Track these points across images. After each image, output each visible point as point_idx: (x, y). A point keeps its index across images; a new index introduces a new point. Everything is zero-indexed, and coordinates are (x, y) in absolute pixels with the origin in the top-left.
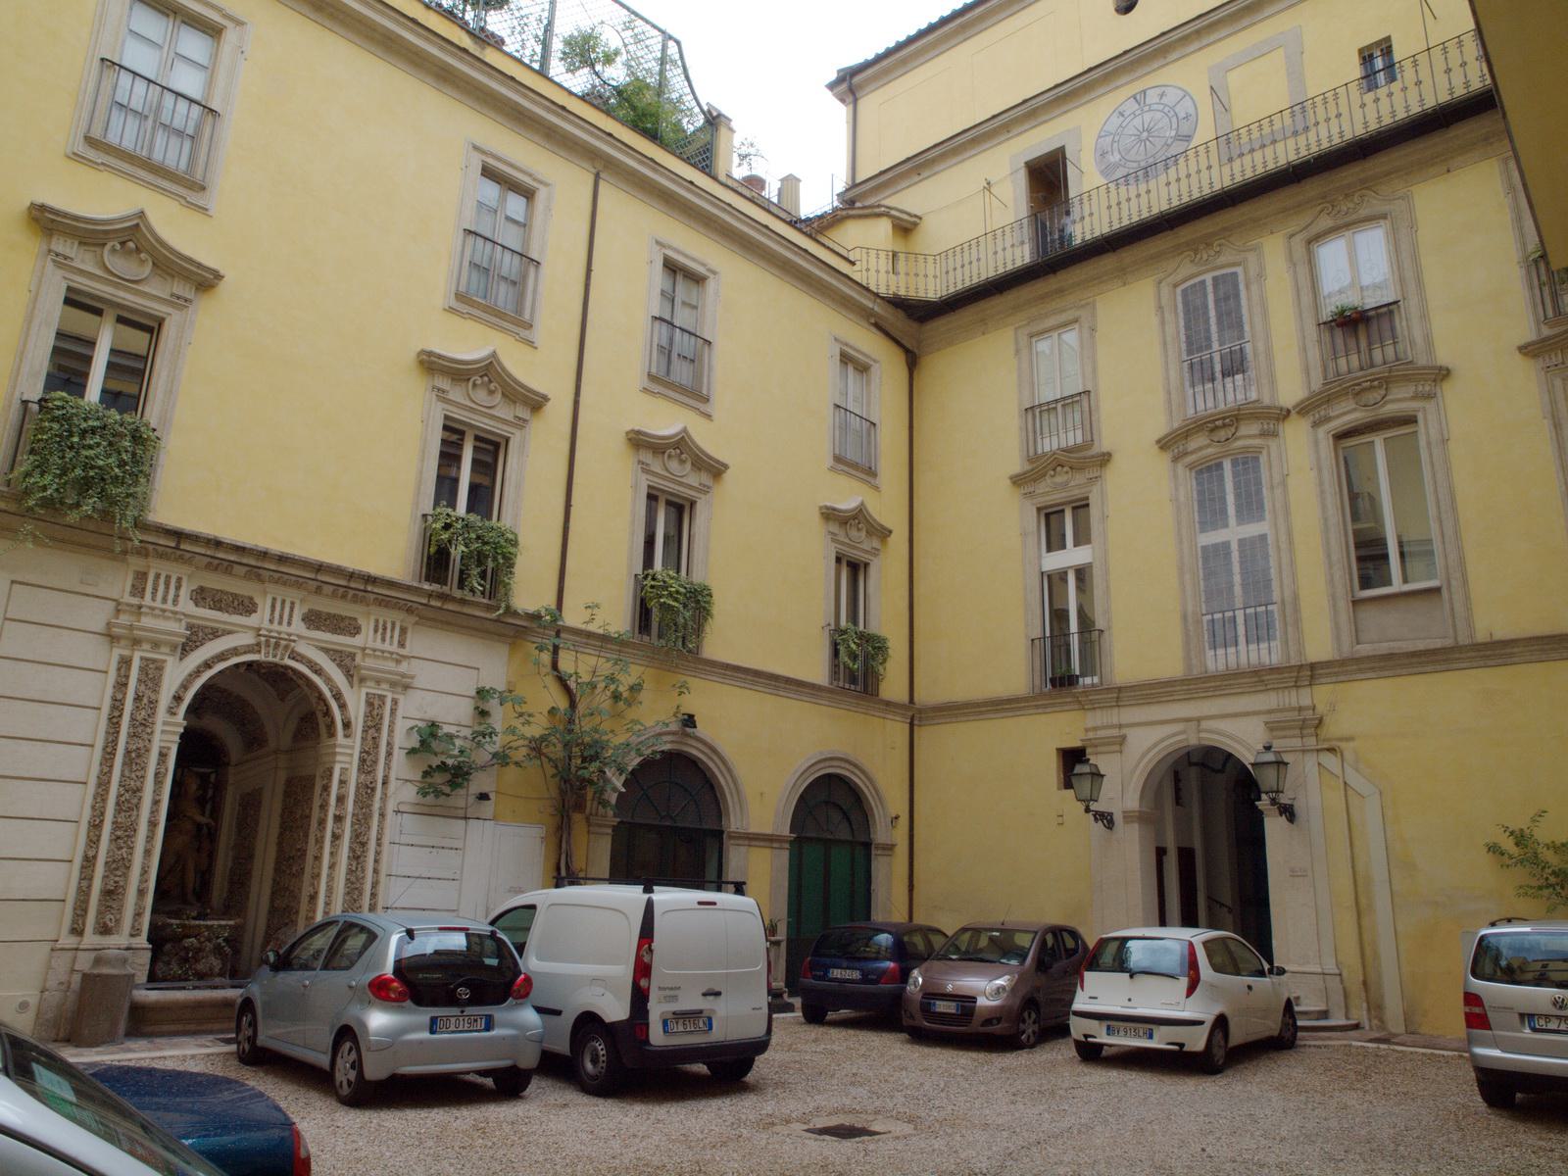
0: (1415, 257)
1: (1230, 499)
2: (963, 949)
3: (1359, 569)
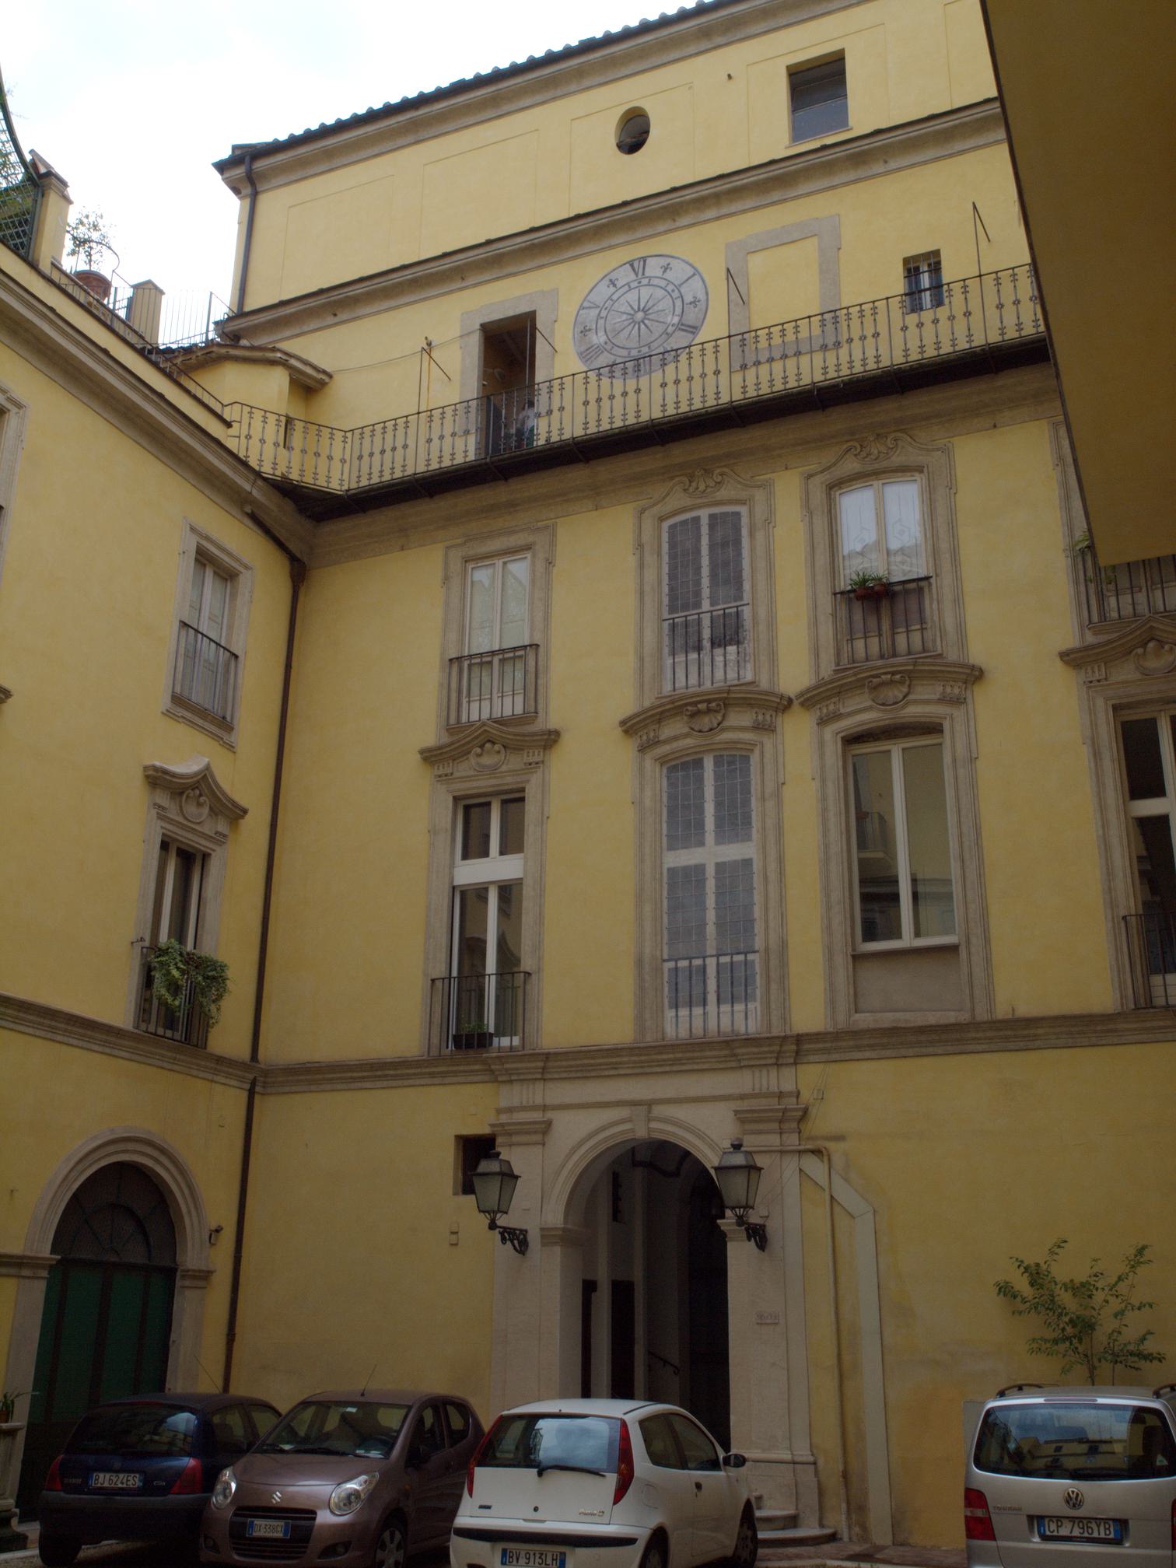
0: (952, 526)
1: (709, 808)
2: (302, 1434)
3: (863, 910)
